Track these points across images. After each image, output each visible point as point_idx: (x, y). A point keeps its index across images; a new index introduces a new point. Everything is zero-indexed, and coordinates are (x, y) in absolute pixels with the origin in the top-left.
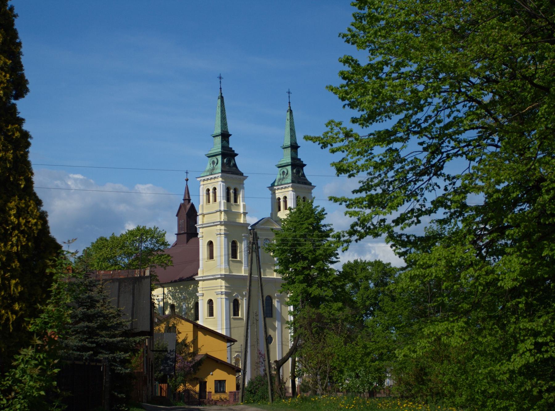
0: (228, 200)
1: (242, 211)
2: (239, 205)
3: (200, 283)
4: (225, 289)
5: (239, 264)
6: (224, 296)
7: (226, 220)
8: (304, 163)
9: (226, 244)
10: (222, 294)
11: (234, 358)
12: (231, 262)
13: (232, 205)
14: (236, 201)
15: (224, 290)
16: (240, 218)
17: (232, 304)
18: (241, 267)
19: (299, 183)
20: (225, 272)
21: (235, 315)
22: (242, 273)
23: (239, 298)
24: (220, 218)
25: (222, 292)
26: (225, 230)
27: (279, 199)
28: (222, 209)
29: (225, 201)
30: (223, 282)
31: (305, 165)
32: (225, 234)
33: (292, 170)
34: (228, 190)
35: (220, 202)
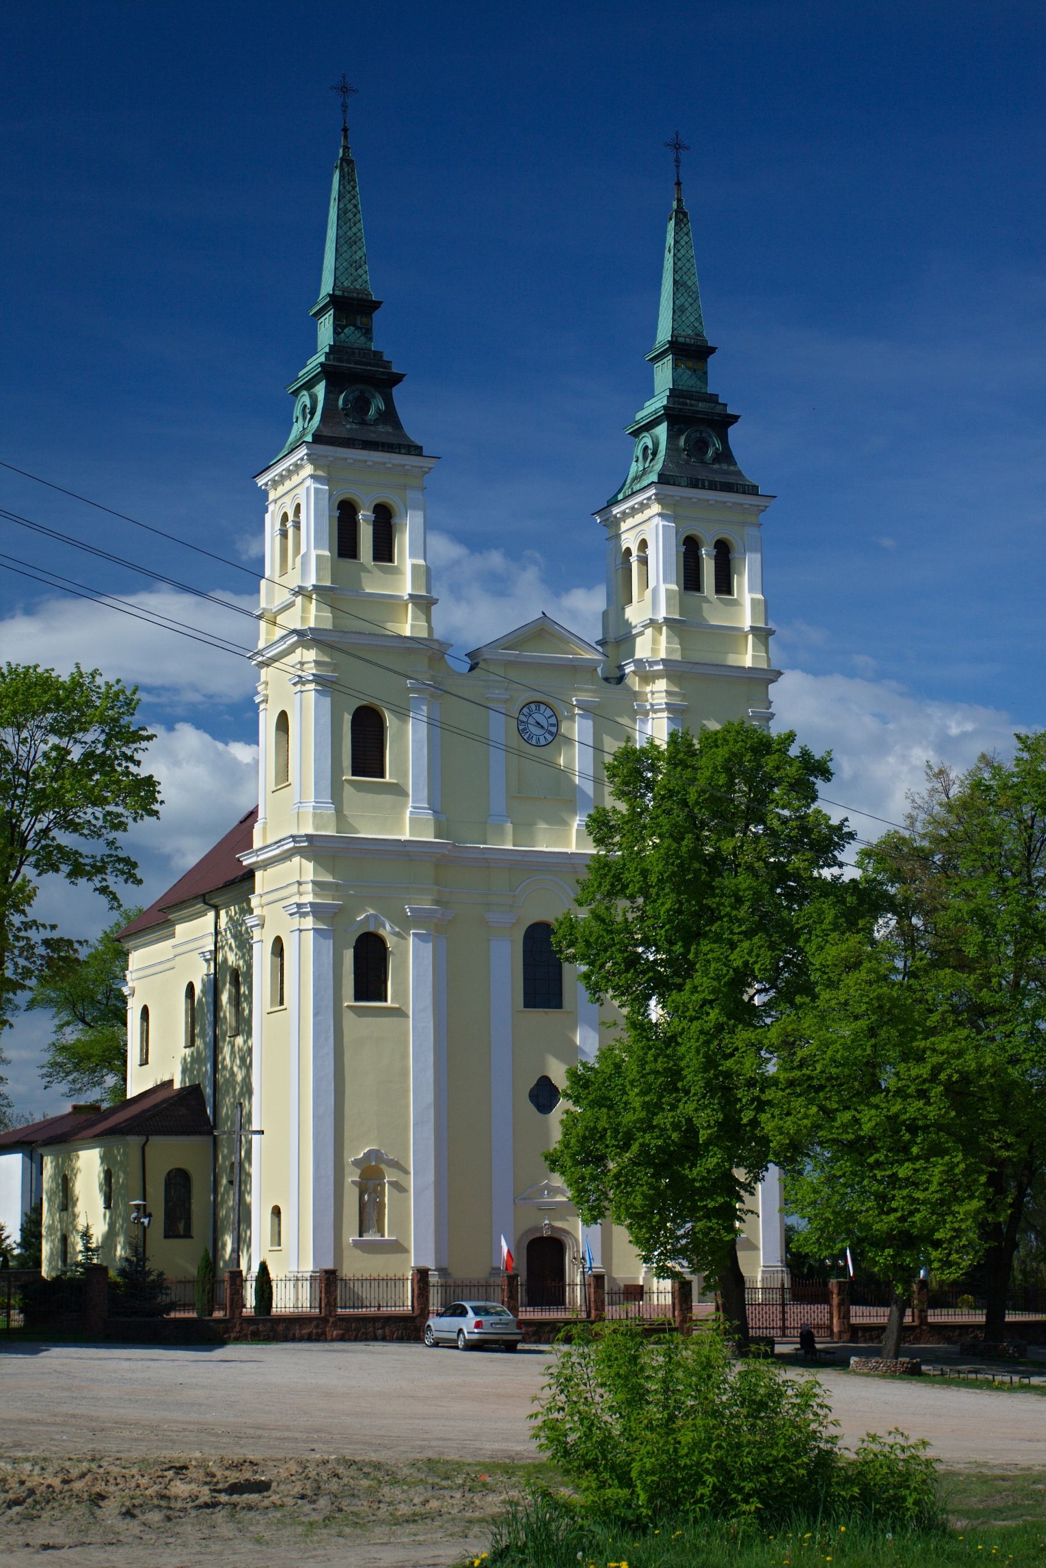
0: (691, 580)
1: (406, 588)
2: (736, 603)
3: (258, 875)
4: (315, 894)
5: (388, 799)
6: (309, 922)
7: (328, 625)
8: (730, 411)
9: (327, 719)
10: (304, 915)
11: (356, 1163)
12: (348, 790)
13: (706, 600)
14: (724, 585)
15: (309, 898)
16: (742, 651)
17: (349, 955)
18: (404, 805)
19: (695, 484)
20: (316, 828)
21: (360, 994)
22: (404, 834)
23: (387, 931)
24: (654, 650)
25: (299, 906)
26: (668, 693)
27: (628, 551)
28: (662, 614)
29: (674, 587)
30: (309, 866)
31: (735, 419)
32: (670, 708)
33: (672, 437)
34: (690, 548)
35: (655, 591)
